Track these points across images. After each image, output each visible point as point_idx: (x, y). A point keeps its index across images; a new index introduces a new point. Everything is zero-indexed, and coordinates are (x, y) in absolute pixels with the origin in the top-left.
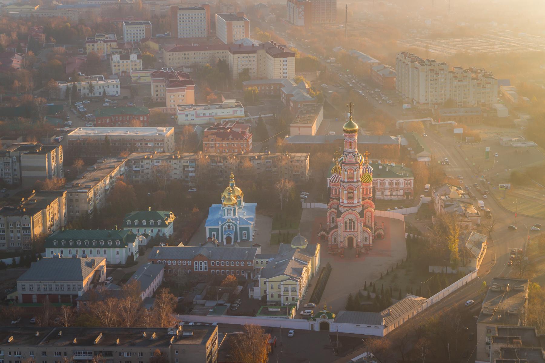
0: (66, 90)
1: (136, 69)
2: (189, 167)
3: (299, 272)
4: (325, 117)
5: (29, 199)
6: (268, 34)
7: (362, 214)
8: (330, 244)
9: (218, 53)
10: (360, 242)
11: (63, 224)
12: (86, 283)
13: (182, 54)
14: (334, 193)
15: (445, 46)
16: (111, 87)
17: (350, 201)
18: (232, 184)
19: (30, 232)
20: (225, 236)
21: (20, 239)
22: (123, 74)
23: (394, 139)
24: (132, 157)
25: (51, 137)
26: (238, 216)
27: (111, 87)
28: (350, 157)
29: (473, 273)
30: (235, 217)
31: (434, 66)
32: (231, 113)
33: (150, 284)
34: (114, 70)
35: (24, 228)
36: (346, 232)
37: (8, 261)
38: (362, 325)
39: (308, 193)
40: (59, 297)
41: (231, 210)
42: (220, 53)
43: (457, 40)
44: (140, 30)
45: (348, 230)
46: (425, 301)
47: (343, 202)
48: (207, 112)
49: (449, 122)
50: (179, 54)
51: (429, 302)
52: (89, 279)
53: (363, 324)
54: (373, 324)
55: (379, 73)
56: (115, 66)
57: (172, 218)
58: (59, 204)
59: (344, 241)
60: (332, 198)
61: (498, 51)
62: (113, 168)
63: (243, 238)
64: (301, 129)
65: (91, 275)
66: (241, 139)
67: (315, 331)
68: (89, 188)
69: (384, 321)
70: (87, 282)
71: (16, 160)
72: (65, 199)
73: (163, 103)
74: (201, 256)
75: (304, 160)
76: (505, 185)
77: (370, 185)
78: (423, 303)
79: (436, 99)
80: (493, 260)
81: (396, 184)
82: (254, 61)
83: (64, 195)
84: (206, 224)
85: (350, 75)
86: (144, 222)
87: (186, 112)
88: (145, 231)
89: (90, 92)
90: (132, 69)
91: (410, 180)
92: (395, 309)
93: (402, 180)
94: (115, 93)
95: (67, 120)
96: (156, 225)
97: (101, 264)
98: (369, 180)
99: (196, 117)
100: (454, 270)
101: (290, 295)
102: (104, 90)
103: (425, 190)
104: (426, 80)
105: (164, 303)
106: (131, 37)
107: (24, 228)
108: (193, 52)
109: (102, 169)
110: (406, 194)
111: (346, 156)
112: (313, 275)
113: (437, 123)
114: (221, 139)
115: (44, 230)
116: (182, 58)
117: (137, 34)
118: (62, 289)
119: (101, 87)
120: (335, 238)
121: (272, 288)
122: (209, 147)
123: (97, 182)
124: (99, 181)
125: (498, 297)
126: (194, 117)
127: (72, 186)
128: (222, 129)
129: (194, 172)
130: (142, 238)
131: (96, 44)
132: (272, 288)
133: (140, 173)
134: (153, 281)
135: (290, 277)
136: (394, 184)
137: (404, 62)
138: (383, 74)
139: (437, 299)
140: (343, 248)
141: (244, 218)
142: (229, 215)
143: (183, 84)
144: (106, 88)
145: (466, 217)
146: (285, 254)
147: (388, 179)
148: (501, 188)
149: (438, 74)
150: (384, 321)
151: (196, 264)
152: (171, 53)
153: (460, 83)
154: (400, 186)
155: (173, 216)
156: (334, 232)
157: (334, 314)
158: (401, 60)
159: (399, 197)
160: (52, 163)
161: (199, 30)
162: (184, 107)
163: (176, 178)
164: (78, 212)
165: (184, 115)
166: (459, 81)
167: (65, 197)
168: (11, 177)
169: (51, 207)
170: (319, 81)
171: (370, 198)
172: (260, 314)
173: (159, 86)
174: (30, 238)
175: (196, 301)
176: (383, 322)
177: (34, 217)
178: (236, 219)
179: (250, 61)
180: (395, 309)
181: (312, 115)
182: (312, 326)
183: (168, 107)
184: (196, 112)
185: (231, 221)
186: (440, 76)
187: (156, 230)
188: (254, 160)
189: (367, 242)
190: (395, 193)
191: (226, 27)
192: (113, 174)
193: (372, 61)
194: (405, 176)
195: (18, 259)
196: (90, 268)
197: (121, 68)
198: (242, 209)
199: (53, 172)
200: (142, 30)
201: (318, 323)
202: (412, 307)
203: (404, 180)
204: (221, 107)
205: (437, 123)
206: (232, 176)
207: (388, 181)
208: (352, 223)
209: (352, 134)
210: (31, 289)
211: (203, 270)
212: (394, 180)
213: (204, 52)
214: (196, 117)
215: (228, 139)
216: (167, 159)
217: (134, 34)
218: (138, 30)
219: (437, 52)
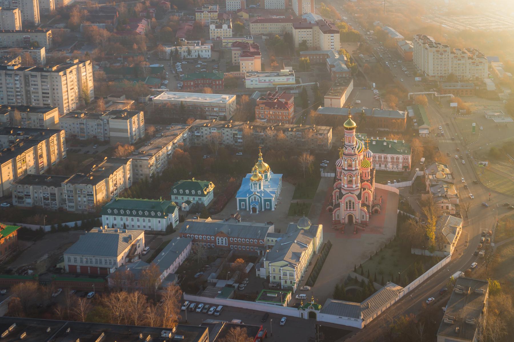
0: (170, 53)
1: (227, 35)
2: (238, 134)
3: (297, 256)
4: (354, 86)
5: (99, 166)
6: (328, 9)
7: (359, 196)
9: (288, 25)
10: (358, 219)
11: (128, 186)
12: (121, 258)
13: (262, 25)
14: (339, 175)
15: (456, 22)
16: (204, 51)
17: (350, 186)
18: (260, 161)
19: (93, 198)
20: (251, 207)
21: (86, 203)
22: (218, 39)
23: (401, 114)
24: (194, 124)
25: (146, 97)
26: (263, 189)
27: (204, 51)
28: (349, 150)
29: (447, 258)
30: (260, 190)
31: (439, 48)
32: (285, 80)
33: (175, 260)
34: (211, 36)
35: (88, 195)
37: (71, 224)
38: (343, 318)
39: (328, 162)
40: (99, 269)
41: (257, 184)
42: (290, 25)
43: (465, 17)
44: (237, 3)
45: (348, 210)
46: (402, 290)
47: (344, 186)
48: (267, 79)
49: (449, 95)
50: (259, 25)
51: (406, 290)
52: (124, 254)
53: (344, 316)
54: (353, 317)
55: (402, 47)
56: (211, 33)
57: (211, 187)
58: (124, 170)
59: (345, 218)
60: (338, 179)
61: (494, 29)
62: (176, 135)
63: (267, 208)
64: (332, 100)
65: (127, 250)
66: (284, 109)
67: (304, 319)
68: (151, 156)
69: (362, 315)
70: (123, 257)
71: (106, 122)
72: (129, 166)
73: (237, 68)
74: (222, 233)
75: (326, 133)
76: (483, 162)
77: (368, 169)
78: (400, 292)
79: (441, 73)
80: (466, 242)
81: (396, 159)
82: (310, 34)
83: (129, 163)
84: (237, 195)
85: (382, 47)
86: (187, 191)
87: (251, 78)
88: (188, 198)
89: (188, 55)
90: (224, 36)
92: (374, 301)
94: (207, 56)
95: (165, 79)
96: (196, 195)
97: (139, 238)
99: (259, 82)
100: (432, 253)
101: (288, 279)
102: (199, 54)
103: (421, 163)
104: (434, 59)
105: (170, 297)
106: (231, 7)
107: (88, 195)
108: (270, 24)
109: (168, 136)
111: (346, 148)
112: (314, 252)
113: (439, 96)
115: (107, 195)
116: (262, 28)
117: (235, 5)
118: (101, 263)
119: (197, 51)
120: (338, 215)
121: (274, 271)
122: (260, 113)
123: (160, 149)
124: (162, 148)
125: (459, 301)
126: (257, 83)
127: (138, 153)
128: (270, 99)
129: (241, 139)
130: (185, 205)
131: (202, 14)
132: (274, 271)
133: (200, 137)
134: (183, 250)
135: (288, 263)
136: (395, 159)
137: (418, 43)
138: (404, 49)
139: (414, 286)
140: (343, 224)
141: (268, 191)
142: (255, 188)
143: (253, 54)
144: (200, 53)
145: (447, 198)
146: (292, 234)
147: (390, 155)
148: (480, 165)
149: (443, 54)
150: (362, 315)
151: (218, 239)
152: (254, 24)
153: (459, 62)
155: (213, 185)
157: (320, 306)
158: (416, 41)
160: (133, 126)
161: (279, 4)
162: (252, 73)
163: (228, 143)
164: (142, 175)
165: (250, 81)
166: (458, 60)
167: (130, 164)
168: (103, 135)
169: (114, 175)
170: (358, 51)
171: (369, 180)
172: (260, 299)
173: (237, 54)
174: (94, 202)
175: (210, 280)
176: (361, 316)
177: (96, 186)
178: (261, 192)
179: (308, 34)
180: (374, 301)
181: (342, 88)
182: (302, 314)
183: (241, 72)
184: (259, 79)
185: (257, 193)
186: (444, 56)
187: (197, 198)
189: (364, 220)
191: (297, 3)
192: (175, 141)
193: (398, 37)
194: (403, 153)
195: (79, 223)
196: (126, 244)
197: (216, 34)
198: (269, 181)
199: (134, 133)
200: (238, 3)
201: (307, 312)
202: (390, 297)
204: (278, 75)
205: (439, 96)
206: (260, 154)
208: (352, 203)
210: (75, 261)
211: (224, 244)
212: (395, 156)
213: (277, 24)
214: (259, 82)
215: (274, 108)
216: (222, 127)
217: (233, 5)
218: (236, 3)
219: (448, 27)
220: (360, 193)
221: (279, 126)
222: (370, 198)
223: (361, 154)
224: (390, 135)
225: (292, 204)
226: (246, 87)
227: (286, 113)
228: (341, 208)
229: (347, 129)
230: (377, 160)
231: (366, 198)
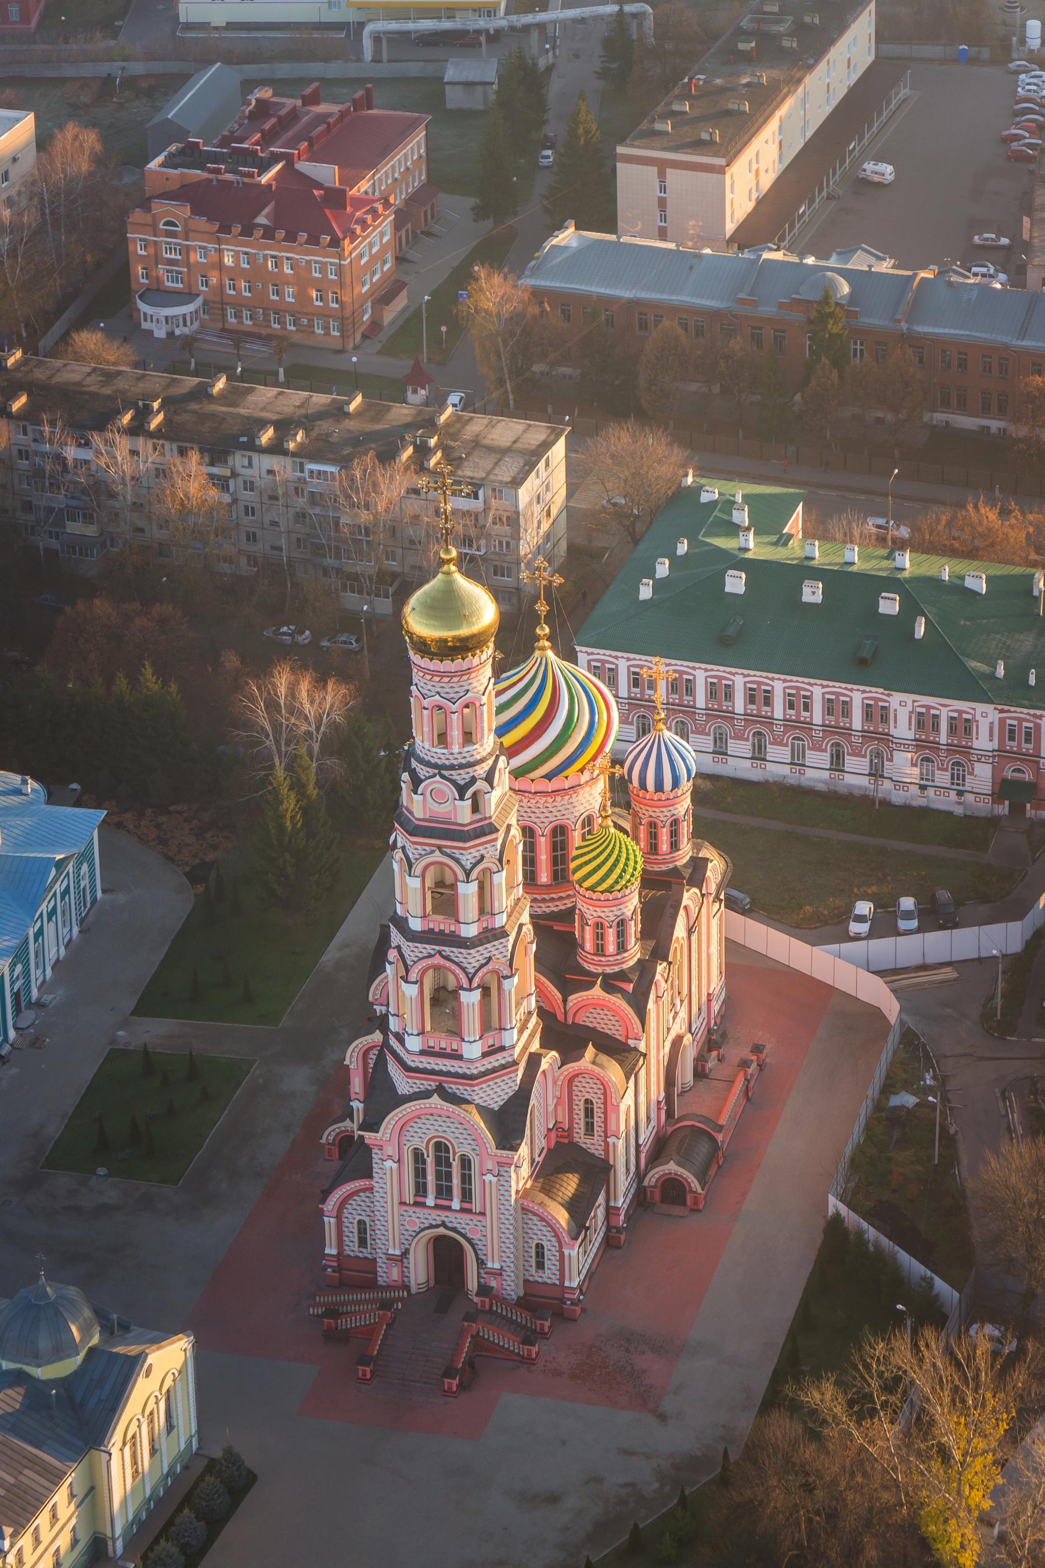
8: (334, 1252)
10: (499, 1273)
36: (417, 1210)
45: (430, 1201)
47: (400, 1038)
59: (405, 1253)
64: (669, 171)
66: (313, 240)
77: (619, 902)
81: (952, 729)
91: (1035, 716)
93: (985, 715)
98: (614, 876)
110: (1004, 789)
114: (216, 226)
122: (157, 259)
147: (908, 698)
154: (976, 744)
156: (356, 1193)
159: (970, 798)
171: (622, 976)
188: (248, 453)
189: (549, 1275)
190: (949, 774)
203: (1002, 711)
207: (909, 708)
208: (456, 1165)
209: (459, 664)
212: (946, 708)
215: (248, 231)
220: (521, 1099)
221: (210, 397)
222: (612, 1117)
223: (585, 777)
224: (976, 507)
225: (116, 1055)
226: (182, 19)
227: (323, 269)
228: (376, 1182)
229: (423, 647)
230: (817, 719)
231: (589, 1113)
